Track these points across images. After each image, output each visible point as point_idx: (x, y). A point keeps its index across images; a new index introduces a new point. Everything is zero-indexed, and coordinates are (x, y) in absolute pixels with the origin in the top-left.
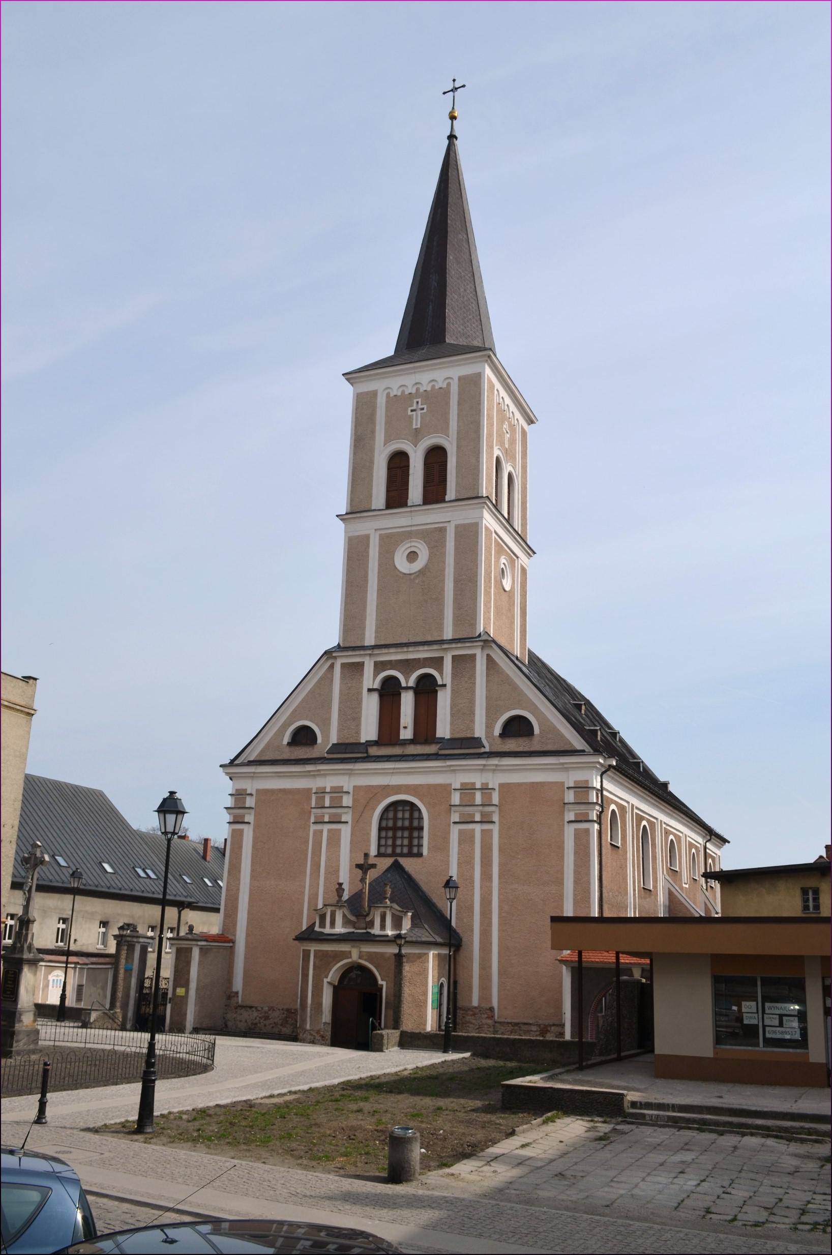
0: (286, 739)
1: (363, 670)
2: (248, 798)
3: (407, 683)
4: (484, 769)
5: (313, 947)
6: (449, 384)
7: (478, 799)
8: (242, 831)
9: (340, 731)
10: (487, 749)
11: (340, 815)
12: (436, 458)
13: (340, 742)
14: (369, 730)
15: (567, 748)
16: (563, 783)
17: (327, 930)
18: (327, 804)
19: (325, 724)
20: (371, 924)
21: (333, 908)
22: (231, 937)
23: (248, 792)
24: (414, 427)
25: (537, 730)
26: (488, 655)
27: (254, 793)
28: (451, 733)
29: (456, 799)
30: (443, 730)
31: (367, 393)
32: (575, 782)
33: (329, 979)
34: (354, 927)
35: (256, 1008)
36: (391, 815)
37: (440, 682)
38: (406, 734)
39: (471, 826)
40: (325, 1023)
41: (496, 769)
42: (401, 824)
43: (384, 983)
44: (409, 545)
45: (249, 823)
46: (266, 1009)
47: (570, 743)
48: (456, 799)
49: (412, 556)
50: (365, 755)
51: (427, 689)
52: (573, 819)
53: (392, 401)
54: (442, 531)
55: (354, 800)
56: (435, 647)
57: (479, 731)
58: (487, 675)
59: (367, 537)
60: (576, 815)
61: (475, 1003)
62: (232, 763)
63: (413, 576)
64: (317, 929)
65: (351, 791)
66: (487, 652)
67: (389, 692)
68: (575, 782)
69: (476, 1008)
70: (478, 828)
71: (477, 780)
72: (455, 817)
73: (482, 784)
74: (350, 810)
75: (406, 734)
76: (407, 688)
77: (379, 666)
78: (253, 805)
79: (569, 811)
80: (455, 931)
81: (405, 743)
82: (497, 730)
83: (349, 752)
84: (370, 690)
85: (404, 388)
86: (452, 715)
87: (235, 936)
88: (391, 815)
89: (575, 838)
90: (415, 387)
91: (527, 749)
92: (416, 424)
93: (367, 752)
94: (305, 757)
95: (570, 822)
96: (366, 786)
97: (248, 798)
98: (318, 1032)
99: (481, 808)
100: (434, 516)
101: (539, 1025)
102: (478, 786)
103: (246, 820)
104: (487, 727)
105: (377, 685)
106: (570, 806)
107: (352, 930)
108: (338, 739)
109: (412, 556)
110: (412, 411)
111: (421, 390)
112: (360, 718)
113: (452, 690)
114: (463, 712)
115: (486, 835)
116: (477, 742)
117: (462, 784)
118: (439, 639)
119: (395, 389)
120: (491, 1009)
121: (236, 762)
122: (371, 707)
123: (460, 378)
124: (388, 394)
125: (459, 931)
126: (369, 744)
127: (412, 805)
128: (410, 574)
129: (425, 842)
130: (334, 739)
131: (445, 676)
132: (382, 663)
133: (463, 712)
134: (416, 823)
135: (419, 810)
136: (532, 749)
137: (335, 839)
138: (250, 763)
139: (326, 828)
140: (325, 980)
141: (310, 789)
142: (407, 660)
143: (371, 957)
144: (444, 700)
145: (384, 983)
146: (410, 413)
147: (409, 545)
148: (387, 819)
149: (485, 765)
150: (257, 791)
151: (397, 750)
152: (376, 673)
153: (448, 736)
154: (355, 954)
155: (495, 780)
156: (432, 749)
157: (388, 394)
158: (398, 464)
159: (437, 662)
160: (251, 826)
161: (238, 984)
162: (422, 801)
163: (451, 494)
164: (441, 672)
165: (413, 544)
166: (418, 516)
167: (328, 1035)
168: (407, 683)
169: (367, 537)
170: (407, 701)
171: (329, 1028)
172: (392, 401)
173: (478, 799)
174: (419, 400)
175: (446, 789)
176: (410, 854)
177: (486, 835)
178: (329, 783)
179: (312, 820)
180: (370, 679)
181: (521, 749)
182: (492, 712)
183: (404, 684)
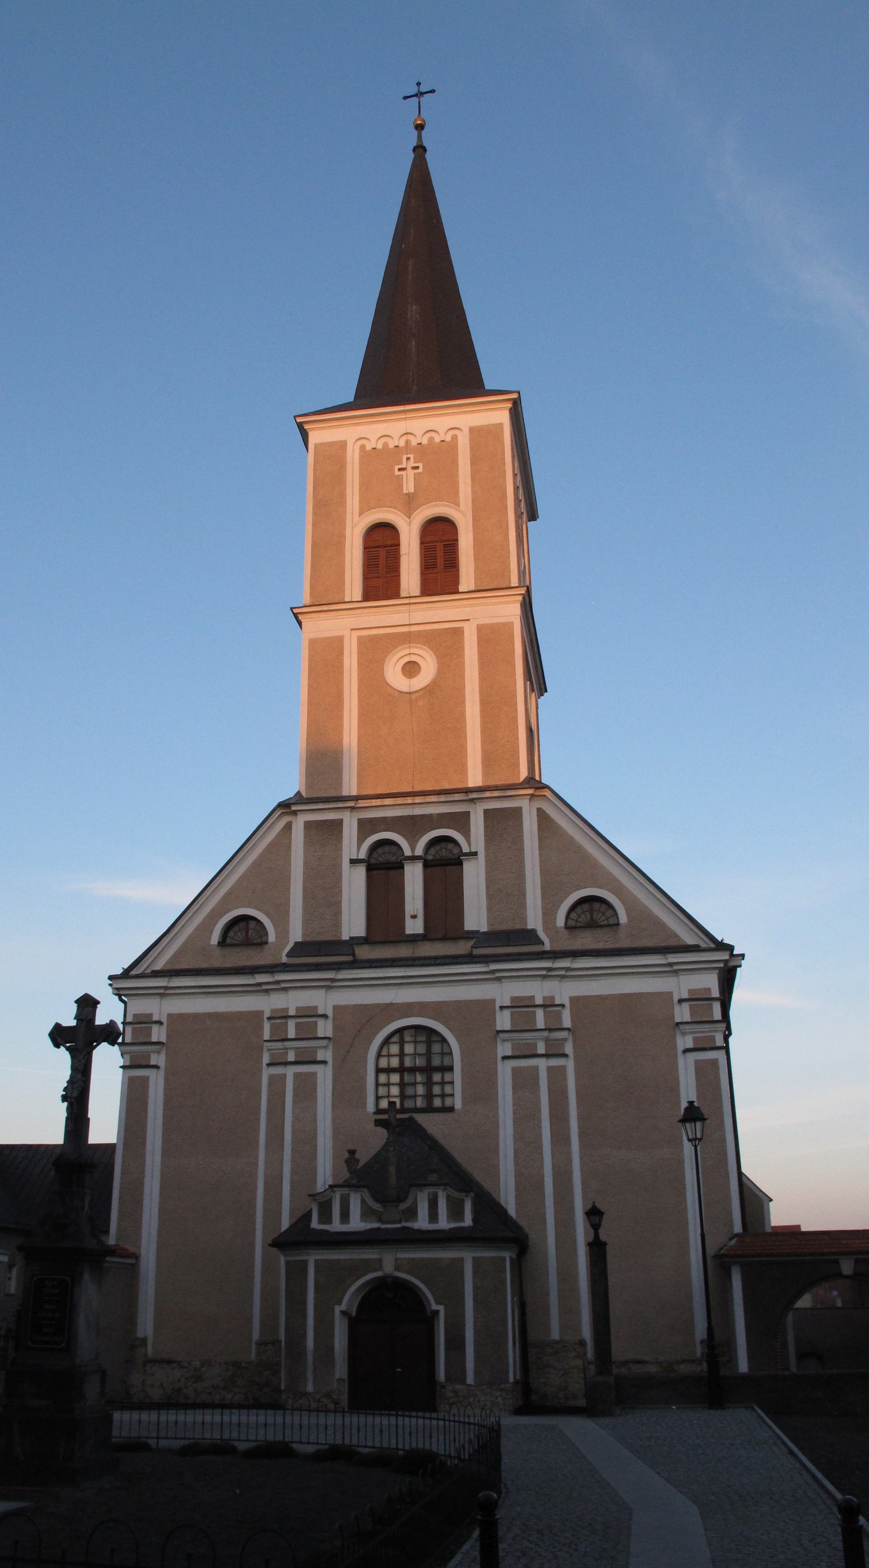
0: (215, 938)
1: (341, 832)
2: (155, 1028)
3: (413, 849)
4: (547, 975)
5: (312, 1258)
6: (455, 438)
7: (540, 1021)
8: (145, 1080)
9: (306, 923)
10: (547, 947)
11: (314, 1050)
12: (440, 538)
13: (309, 939)
14: (353, 922)
15: (672, 942)
16: (670, 994)
17: (336, 1226)
18: (292, 1034)
19: (281, 914)
20: (412, 1213)
21: (345, 1191)
22: (132, 1249)
23: (155, 1018)
24: (405, 491)
25: (623, 918)
26: (539, 810)
27: (164, 1020)
28: (489, 923)
29: (504, 1021)
30: (476, 916)
31: (331, 444)
32: (690, 991)
33: (343, 1307)
34: (380, 1220)
35: (179, 1363)
36: (394, 1049)
37: (466, 849)
38: (414, 926)
40: (340, 1380)
41: (566, 976)
43: (441, 1308)
44: (407, 651)
45: (324, 1062)
46: (197, 1363)
47: (676, 936)
48: (504, 1021)
49: (411, 669)
50: (350, 958)
51: (444, 863)
52: (510, 1054)
53: (369, 457)
54: (457, 633)
55: (335, 1028)
56: (457, 797)
57: (534, 920)
58: (540, 839)
59: (340, 640)
60: (695, 1040)
61: (555, 1335)
62: (126, 974)
63: (414, 696)
64: (315, 1224)
65: (330, 1013)
66: (538, 804)
67: (383, 867)
68: (690, 991)
69: (557, 1342)
70: (542, 1064)
71: (537, 990)
72: (685, 1041)
73: (544, 998)
75: (414, 926)
76: (414, 858)
77: (366, 827)
78: (329, 1034)
79: (504, 1041)
80: (515, 1224)
81: (414, 939)
82: (560, 921)
83: (323, 954)
84: (353, 862)
85: (410, 437)
86: (490, 897)
87: (139, 1247)
88: (394, 1049)
89: (697, 1073)
90: (404, 438)
91: (609, 946)
92: (409, 486)
93: (353, 955)
94: (248, 963)
95: (505, 1058)
96: (355, 1006)
97: (155, 1028)
98: (328, 1395)
99: (546, 1034)
100: (441, 612)
102: (539, 1001)
103: (152, 1063)
104: (545, 914)
105: (363, 855)
106: (687, 1027)
107: (376, 1225)
108: (304, 935)
109: (411, 669)
110: (400, 470)
111: (368, 448)
112: (340, 902)
113: (488, 860)
114: (505, 890)
115: (557, 1076)
116: (530, 936)
117: (513, 999)
118: (460, 786)
119: (442, 431)
120: (582, 1343)
121: (133, 972)
122: (354, 885)
123: (472, 430)
124: (363, 447)
125: (523, 1223)
126: (355, 941)
127: (430, 1031)
128: (410, 693)
130: (296, 934)
131: (476, 838)
132: (371, 821)
133: (505, 890)
134: (436, 1061)
135: (444, 1040)
136: (617, 946)
137: (306, 1089)
138: (156, 974)
139: (290, 1072)
140: (337, 1309)
141: (261, 1013)
142: (412, 817)
143: (415, 1267)
144: (474, 877)
146: (397, 473)
147: (407, 651)
148: (389, 1056)
149: (550, 969)
150: (170, 1016)
151: (404, 951)
153: (484, 928)
154: (389, 1262)
155: (564, 992)
156: (462, 948)
157: (363, 447)
158: (381, 542)
159: (461, 821)
161: (146, 1324)
162: (447, 1026)
164: (467, 835)
165: (413, 651)
166: (413, 611)
167: (344, 1398)
168: (413, 849)
169: (340, 640)
170: (414, 878)
171: (345, 1388)
172: (369, 457)
173: (540, 1021)
174: (411, 456)
175: (486, 1007)
176: (430, 1109)
177: (557, 1076)
178: (293, 1001)
179: (266, 1059)
180: (352, 845)
181: (601, 946)
182: (551, 894)
183: (408, 852)
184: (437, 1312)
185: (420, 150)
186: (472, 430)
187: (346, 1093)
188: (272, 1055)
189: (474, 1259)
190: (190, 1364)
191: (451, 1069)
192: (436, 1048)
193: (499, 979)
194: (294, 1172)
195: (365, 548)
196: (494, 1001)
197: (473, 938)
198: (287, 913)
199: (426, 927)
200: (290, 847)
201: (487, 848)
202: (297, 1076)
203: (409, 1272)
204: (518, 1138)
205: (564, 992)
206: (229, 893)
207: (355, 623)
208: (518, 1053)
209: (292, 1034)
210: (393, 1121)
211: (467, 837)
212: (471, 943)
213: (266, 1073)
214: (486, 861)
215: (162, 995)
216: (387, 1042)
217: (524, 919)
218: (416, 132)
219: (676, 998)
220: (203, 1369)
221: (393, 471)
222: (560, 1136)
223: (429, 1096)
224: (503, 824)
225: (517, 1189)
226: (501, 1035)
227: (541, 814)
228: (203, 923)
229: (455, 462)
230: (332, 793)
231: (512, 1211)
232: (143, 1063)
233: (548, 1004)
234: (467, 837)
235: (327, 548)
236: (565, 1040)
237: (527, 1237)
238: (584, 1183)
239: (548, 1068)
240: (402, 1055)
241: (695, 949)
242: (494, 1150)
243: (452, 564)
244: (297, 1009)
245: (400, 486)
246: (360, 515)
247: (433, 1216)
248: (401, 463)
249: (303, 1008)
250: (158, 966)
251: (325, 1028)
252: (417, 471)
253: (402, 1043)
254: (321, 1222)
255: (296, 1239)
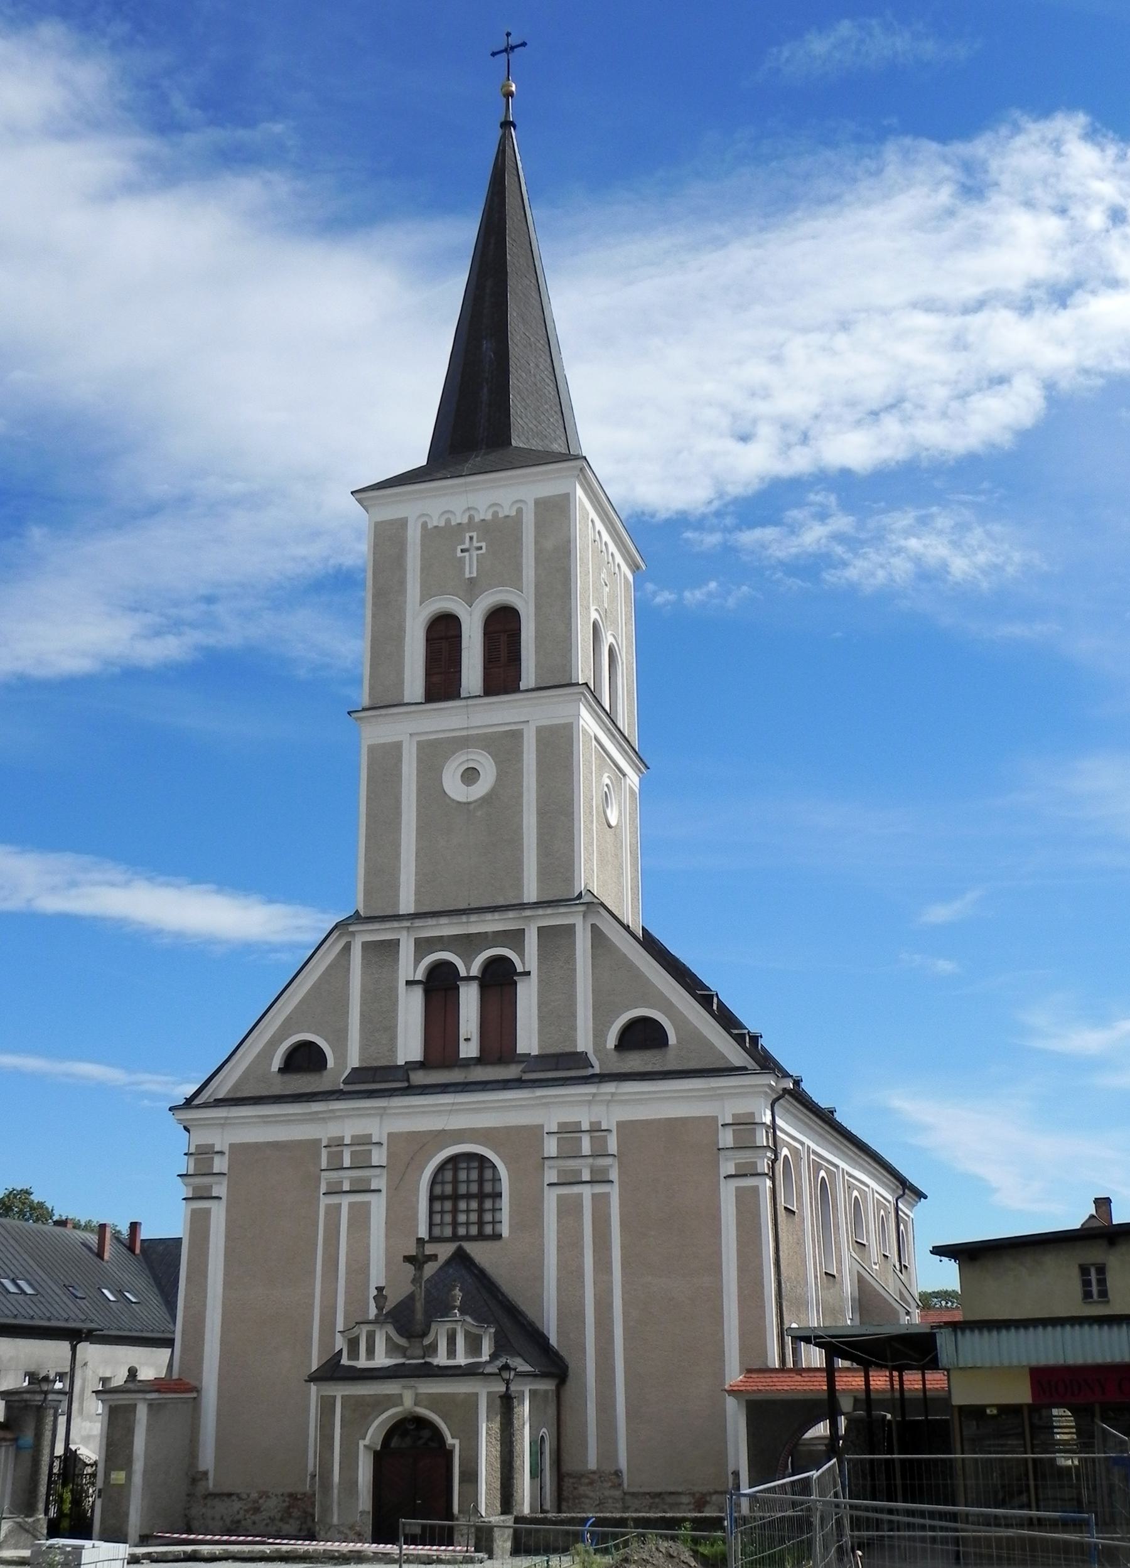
0: (277, 1063)
3: (468, 970)
5: (340, 1391)
6: (520, 511)
7: (586, 1147)
8: (207, 1212)
9: (363, 1048)
11: (368, 1180)
12: (503, 625)
13: (365, 1065)
14: (410, 1045)
17: (362, 1363)
18: (347, 1163)
19: (340, 1039)
20: (432, 1349)
22: (193, 1383)
24: (467, 576)
27: (226, 1150)
28: (540, 1047)
29: (551, 1147)
31: (391, 522)
34: (405, 1356)
36: (448, 1175)
37: (520, 969)
38: (469, 1049)
39: (576, 1189)
42: (465, 1185)
43: (456, 1442)
44: (464, 758)
46: (254, 1495)
47: (724, 1057)
49: (470, 775)
50: (406, 1084)
51: (499, 980)
53: (430, 535)
54: (515, 736)
55: (390, 1156)
57: (584, 1042)
58: (594, 957)
59: (398, 746)
62: (189, 1103)
63: (472, 807)
64: (345, 1361)
65: (385, 1141)
67: (440, 986)
69: (594, 1473)
70: (587, 1191)
73: (591, 1123)
74: (385, 1171)
75: (469, 1049)
76: (469, 979)
77: (423, 946)
80: (556, 1354)
81: (468, 1063)
82: (611, 1041)
83: (379, 1080)
84: (409, 983)
85: (472, 512)
88: (448, 1175)
93: (408, 1080)
94: (308, 1091)
99: (590, 1160)
100: (502, 713)
101: (693, 1494)
104: (595, 1036)
105: (420, 975)
109: (470, 775)
110: (462, 551)
114: (556, 1013)
115: (600, 1202)
116: (581, 1059)
120: (618, 1473)
121: (196, 1102)
122: (411, 1010)
123: (538, 503)
126: (411, 1066)
127: (482, 1159)
128: (469, 803)
129: (505, 1216)
131: (529, 959)
133: (556, 1013)
134: (488, 1188)
135: (494, 1167)
138: (219, 1103)
139: (345, 1201)
140: (362, 1443)
142: (469, 935)
144: (527, 996)
145: (456, 1442)
146: (459, 554)
147: (464, 758)
148: (443, 1183)
152: (417, 962)
158: (443, 633)
159: (515, 938)
160: (616, 1185)
163: (528, 677)
168: (468, 970)
169: (398, 746)
170: (469, 999)
172: (430, 535)
173: (586, 1147)
174: (474, 534)
175: (535, 1133)
176: (481, 1237)
177: (600, 1202)
178: (349, 1130)
179: (323, 1189)
180: (409, 966)
183: (463, 973)
184: (454, 1446)
185: (501, 153)
186: (538, 503)
187: (397, 1221)
188: (328, 1184)
189: (489, 1393)
190: (248, 1496)
191: (500, 1195)
192: (488, 1174)
193: (546, 1104)
194: (347, 1303)
195: (427, 640)
196: (542, 1126)
197: (523, 1062)
198: (346, 1039)
199: (482, 1049)
200: (349, 969)
201: (539, 968)
202: (352, 1205)
203: (426, 1408)
204: (562, 1266)
205: (611, 1118)
206: (289, 1019)
207: (414, 727)
208: (561, 1181)
209: (347, 1163)
210: (420, 1257)
211: (521, 955)
212: (521, 1067)
213: (324, 1201)
214: (539, 982)
215: (222, 1125)
216: (441, 1168)
217: (574, 1041)
218: (500, 132)
219: (720, 1123)
220: (261, 1501)
221: (455, 550)
222: (603, 1265)
223: (481, 1223)
224: (556, 940)
225: (559, 1319)
226: (547, 1162)
227: (595, 930)
228: (263, 1050)
229: (519, 540)
230: (389, 912)
231: (553, 1341)
232: (205, 1195)
233: (595, 1129)
234: (521, 955)
235: (385, 646)
236: (611, 1166)
237: (567, 1367)
238: (626, 1314)
239: (593, 1195)
240: (455, 1182)
241: (740, 1070)
242: (539, 1278)
243: (515, 658)
244: (353, 1137)
245: (462, 570)
246: (421, 603)
247: (452, 1353)
248: (464, 543)
249: (357, 1136)
250: (221, 1095)
251: (379, 1157)
252: (480, 552)
253: (456, 1170)
254: (349, 1359)
255: (333, 1371)
